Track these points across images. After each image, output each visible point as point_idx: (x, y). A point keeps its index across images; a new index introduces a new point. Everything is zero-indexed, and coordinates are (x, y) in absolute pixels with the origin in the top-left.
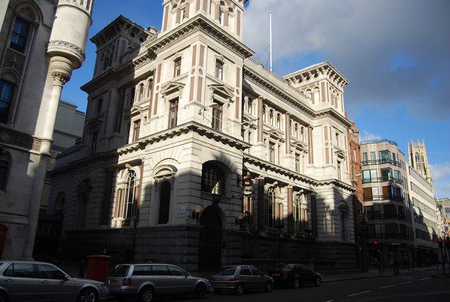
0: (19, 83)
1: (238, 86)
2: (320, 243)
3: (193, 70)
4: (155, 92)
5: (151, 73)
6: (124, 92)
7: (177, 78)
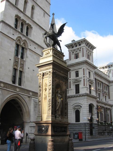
3: (84, 77)
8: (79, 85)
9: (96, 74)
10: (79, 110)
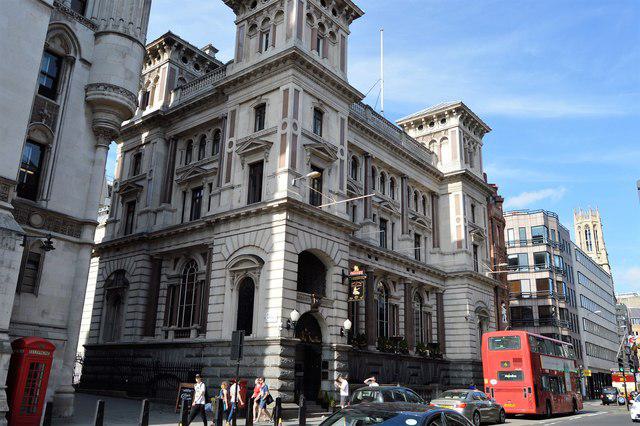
0: (52, 143)
1: (342, 144)
2: (448, 363)
3: (285, 125)
4: (227, 150)
5: (221, 120)
6: (176, 145)
7: (261, 133)
8: (260, 164)
9: (353, 122)
10: (254, 277)
